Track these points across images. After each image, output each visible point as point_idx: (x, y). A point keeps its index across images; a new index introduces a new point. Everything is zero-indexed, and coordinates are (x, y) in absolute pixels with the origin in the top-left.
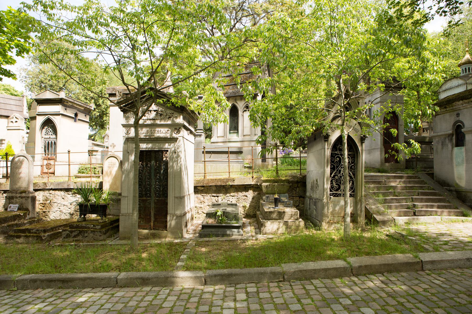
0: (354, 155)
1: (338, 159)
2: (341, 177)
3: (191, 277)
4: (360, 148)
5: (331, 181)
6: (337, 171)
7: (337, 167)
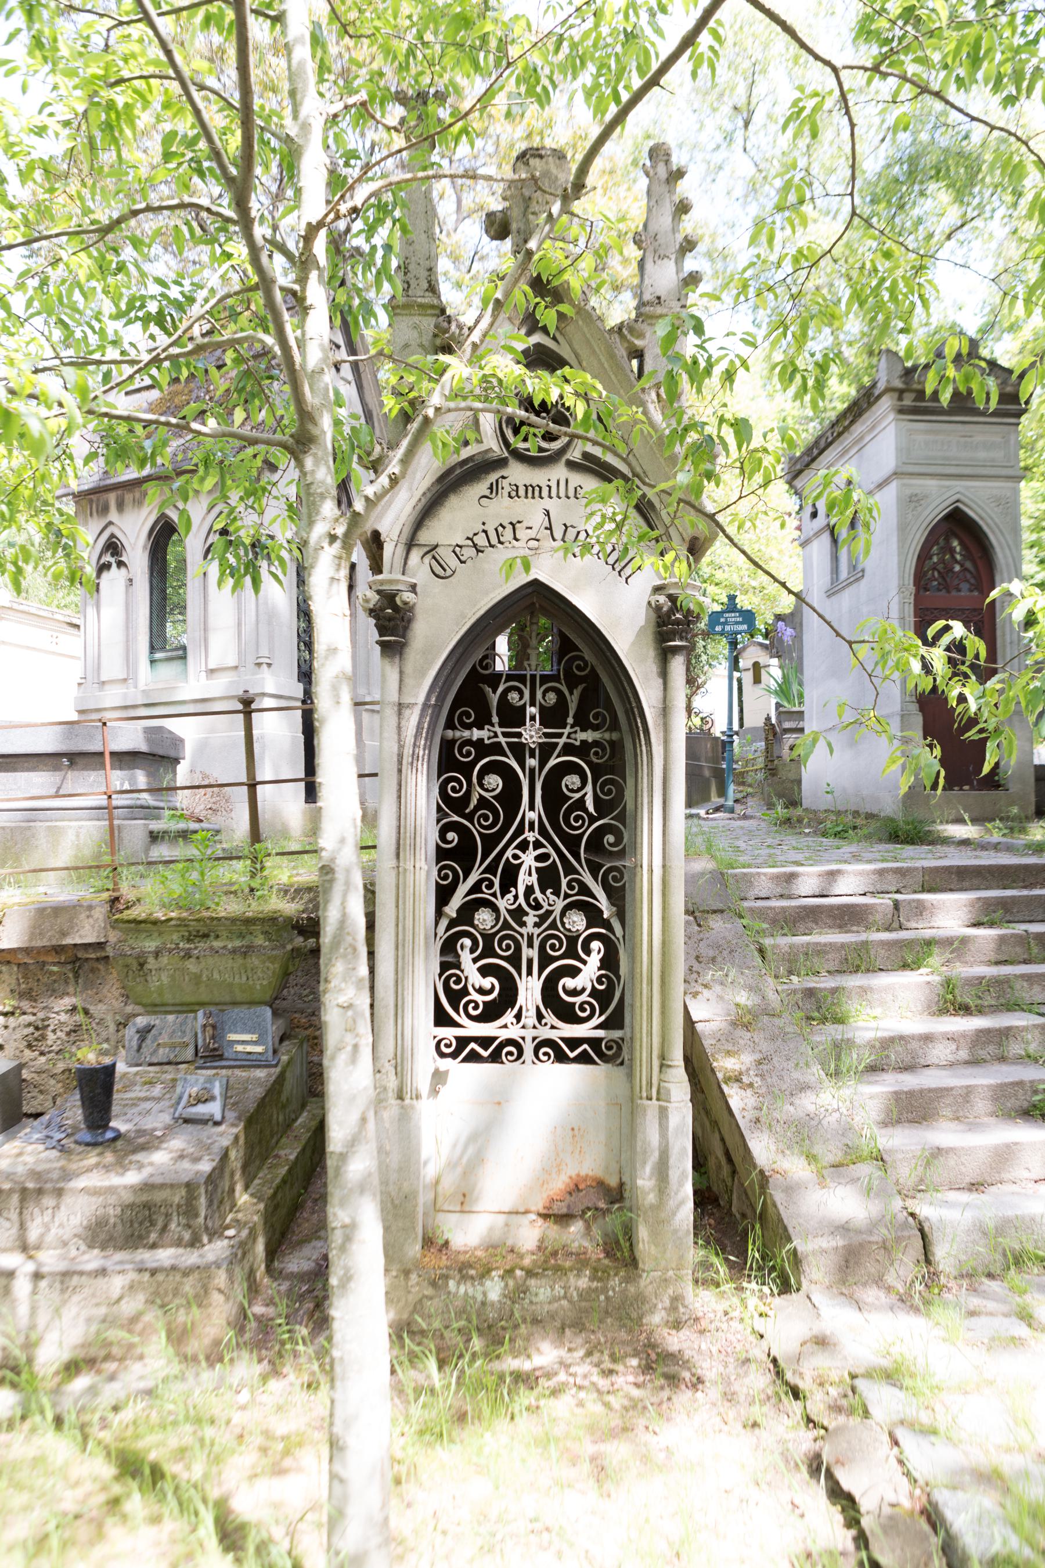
0: (616, 747)
1: (494, 781)
2: (518, 914)
3: (768, 718)
4: (649, 695)
5: (449, 947)
6: (491, 869)
7: (490, 842)
